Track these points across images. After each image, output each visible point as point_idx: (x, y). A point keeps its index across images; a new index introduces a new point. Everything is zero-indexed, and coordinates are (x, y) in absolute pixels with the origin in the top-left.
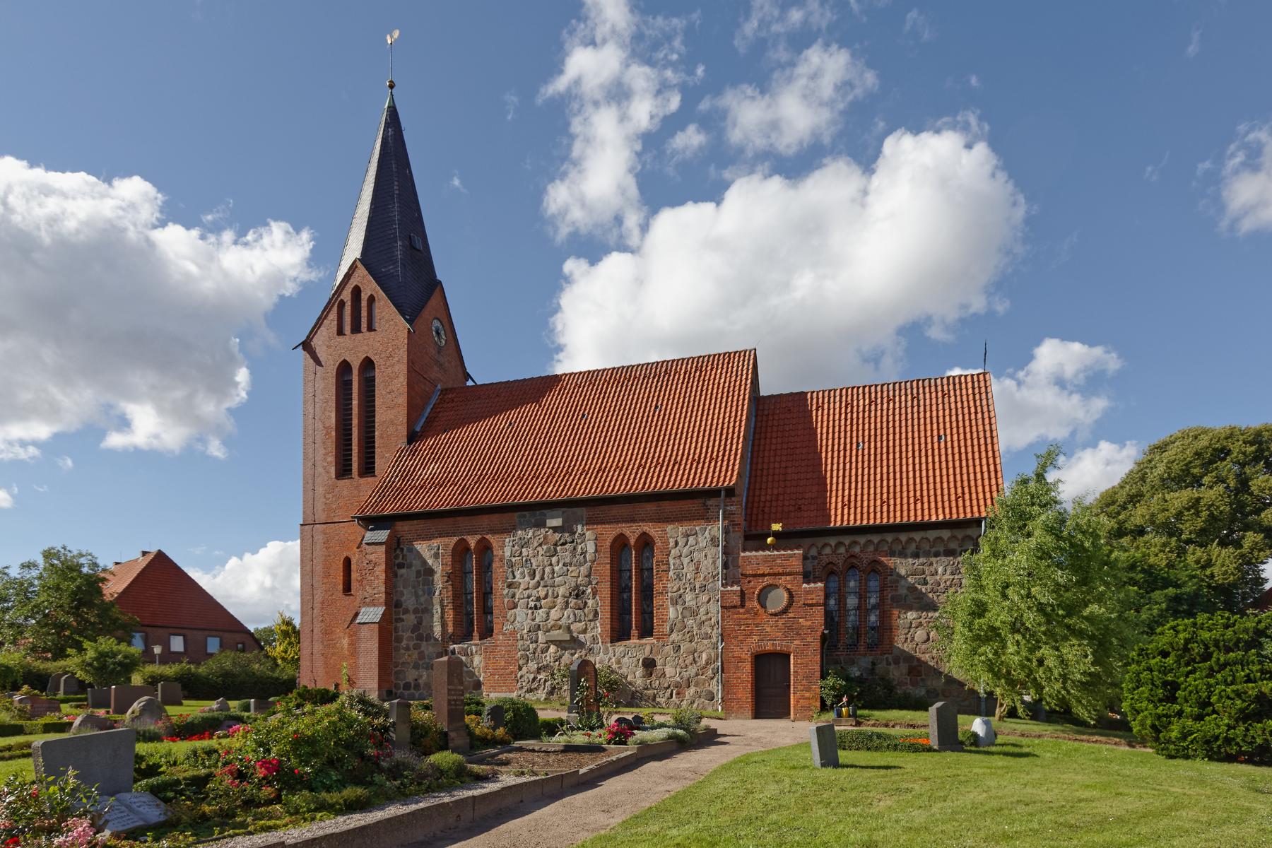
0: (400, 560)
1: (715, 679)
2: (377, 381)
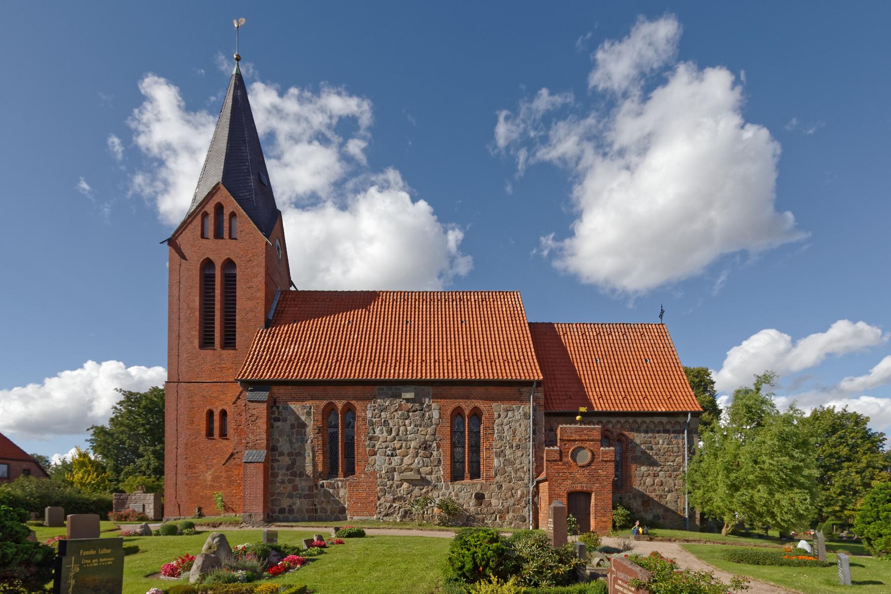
0: (276, 415)
1: (527, 508)
2: (238, 278)
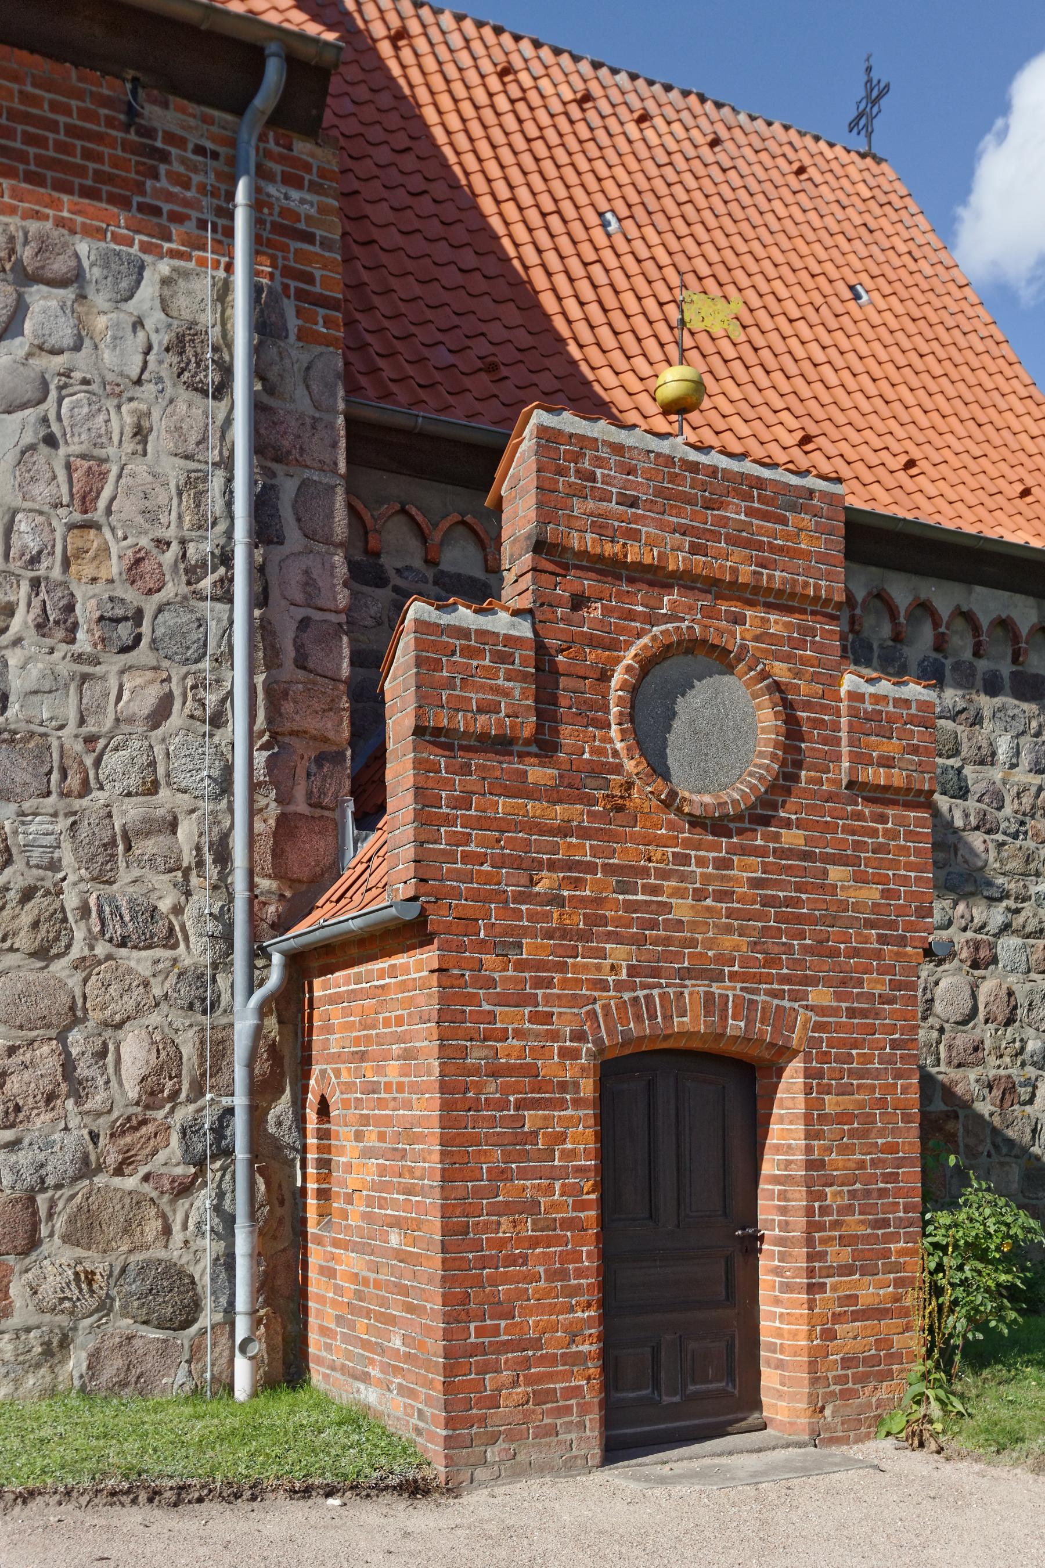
1: (204, 1198)
